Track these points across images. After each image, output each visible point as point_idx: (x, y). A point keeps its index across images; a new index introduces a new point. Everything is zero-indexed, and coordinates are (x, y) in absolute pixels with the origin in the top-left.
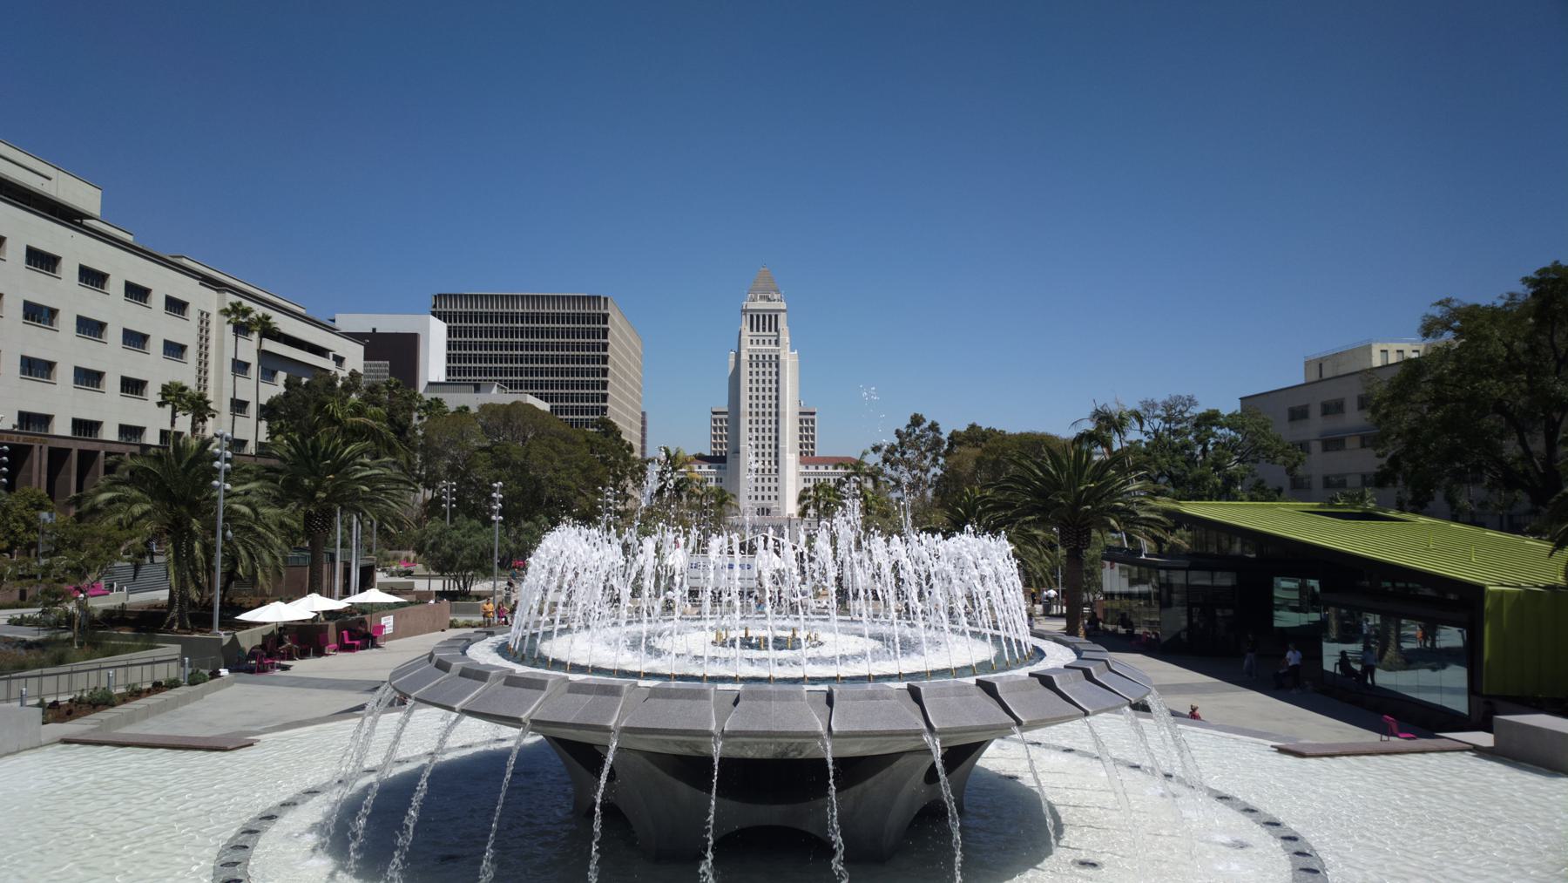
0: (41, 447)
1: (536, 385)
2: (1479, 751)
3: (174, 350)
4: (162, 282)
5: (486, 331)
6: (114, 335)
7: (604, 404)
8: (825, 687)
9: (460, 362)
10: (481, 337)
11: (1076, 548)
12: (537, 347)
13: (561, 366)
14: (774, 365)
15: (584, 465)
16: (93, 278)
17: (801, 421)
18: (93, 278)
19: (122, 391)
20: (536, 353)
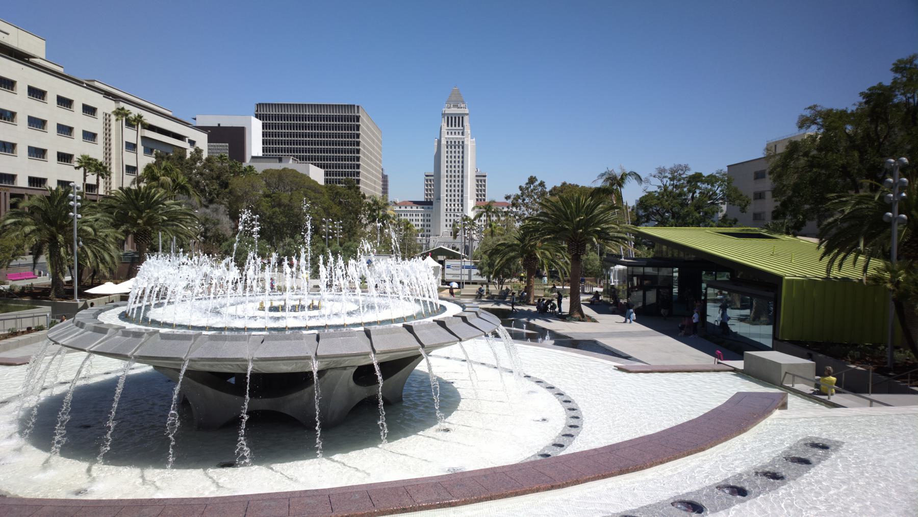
0: (5, 193)
1: (318, 159)
2: (735, 370)
3: (89, 136)
4: (81, 96)
5: (300, 126)
6: (52, 127)
7: (358, 170)
8: (316, 332)
9: (273, 144)
10: (272, 129)
11: (576, 254)
12: (318, 135)
13: (311, 147)
14: (461, 147)
15: (325, 206)
16: (37, 93)
17: (477, 181)
18: (37, 93)
19: (58, 160)
20: (317, 139)
